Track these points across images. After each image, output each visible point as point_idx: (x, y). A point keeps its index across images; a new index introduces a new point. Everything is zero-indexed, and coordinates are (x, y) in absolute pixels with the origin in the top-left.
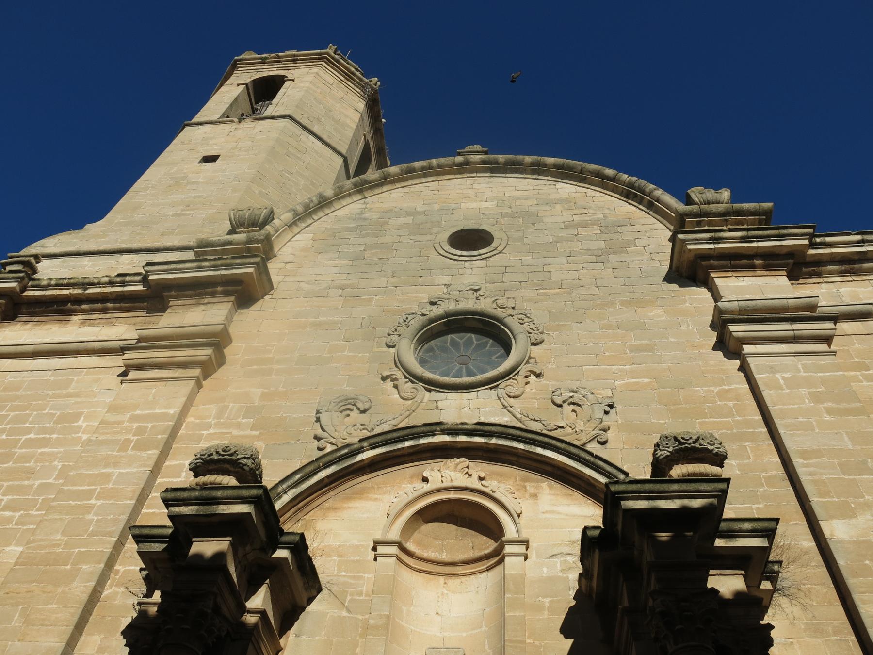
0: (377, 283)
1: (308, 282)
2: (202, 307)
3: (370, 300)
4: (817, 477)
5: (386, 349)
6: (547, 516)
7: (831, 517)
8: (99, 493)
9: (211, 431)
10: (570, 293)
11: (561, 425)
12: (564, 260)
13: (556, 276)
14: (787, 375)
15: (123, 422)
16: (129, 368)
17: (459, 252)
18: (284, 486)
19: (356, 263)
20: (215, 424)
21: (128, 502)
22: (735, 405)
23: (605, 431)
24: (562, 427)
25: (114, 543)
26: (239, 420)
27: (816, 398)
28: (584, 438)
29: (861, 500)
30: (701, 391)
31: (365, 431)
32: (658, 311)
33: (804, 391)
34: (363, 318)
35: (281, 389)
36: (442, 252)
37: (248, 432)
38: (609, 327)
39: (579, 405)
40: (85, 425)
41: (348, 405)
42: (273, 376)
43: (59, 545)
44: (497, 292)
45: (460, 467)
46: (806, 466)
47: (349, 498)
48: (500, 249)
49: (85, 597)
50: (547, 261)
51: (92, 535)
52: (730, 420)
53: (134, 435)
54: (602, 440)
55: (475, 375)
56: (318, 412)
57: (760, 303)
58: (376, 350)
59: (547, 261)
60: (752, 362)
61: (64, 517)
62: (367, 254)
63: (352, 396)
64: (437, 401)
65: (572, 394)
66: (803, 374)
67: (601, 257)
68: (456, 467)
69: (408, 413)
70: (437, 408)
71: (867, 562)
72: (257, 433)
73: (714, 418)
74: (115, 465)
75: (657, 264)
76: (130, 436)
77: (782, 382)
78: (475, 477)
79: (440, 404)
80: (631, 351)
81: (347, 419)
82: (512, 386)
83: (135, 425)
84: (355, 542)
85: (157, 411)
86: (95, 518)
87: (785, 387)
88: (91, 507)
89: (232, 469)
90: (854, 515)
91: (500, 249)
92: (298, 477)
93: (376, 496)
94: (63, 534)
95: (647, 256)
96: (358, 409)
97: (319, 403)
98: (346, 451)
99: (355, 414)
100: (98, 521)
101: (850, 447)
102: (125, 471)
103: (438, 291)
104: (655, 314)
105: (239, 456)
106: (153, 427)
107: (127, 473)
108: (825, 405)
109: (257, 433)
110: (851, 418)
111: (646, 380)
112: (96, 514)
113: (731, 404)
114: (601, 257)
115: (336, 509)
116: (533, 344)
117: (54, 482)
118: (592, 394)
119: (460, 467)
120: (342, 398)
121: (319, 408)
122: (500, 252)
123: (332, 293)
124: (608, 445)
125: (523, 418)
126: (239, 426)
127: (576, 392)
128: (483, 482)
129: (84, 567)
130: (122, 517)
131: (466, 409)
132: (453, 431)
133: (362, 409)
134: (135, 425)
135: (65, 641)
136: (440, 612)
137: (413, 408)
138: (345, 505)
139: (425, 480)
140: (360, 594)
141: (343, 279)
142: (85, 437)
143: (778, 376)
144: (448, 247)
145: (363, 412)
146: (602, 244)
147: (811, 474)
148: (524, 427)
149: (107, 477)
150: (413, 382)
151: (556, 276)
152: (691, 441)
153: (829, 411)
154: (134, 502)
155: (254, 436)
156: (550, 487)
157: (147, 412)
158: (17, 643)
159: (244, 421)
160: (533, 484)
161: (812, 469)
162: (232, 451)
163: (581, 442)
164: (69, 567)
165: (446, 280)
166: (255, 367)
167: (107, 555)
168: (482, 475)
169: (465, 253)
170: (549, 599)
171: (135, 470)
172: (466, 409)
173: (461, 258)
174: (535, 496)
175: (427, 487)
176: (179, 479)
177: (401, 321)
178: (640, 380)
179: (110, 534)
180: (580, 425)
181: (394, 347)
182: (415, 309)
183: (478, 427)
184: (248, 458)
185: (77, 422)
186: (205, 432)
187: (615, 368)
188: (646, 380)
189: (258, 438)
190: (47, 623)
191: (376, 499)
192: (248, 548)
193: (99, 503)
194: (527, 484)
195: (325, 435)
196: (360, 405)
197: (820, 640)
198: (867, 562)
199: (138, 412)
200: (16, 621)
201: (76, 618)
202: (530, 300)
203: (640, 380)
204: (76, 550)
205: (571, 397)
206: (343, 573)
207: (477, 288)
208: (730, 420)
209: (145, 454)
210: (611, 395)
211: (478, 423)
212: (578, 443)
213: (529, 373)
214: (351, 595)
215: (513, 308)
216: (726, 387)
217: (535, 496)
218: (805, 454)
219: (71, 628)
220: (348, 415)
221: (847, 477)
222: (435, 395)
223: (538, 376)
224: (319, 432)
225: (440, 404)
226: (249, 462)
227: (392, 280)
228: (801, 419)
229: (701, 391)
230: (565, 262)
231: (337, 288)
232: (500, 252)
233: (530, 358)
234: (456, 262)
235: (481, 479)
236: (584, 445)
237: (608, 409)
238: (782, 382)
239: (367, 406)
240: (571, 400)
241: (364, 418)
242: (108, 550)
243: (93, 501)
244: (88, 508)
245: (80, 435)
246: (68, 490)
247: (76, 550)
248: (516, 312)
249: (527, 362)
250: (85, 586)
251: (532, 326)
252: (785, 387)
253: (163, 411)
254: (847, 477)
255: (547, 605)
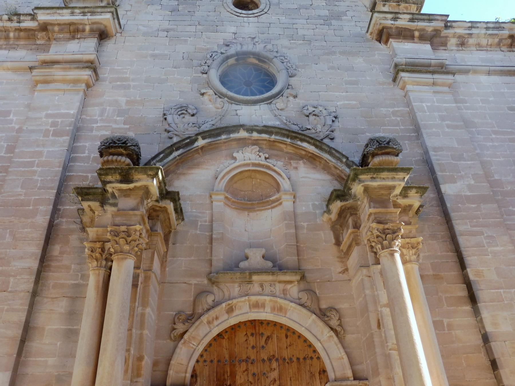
0: (189, 28)
1: (144, 26)
2: (77, 41)
3: (186, 41)
4: (440, 162)
5: (201, 75)
6: (303, 179)
7: (446, 183)
8: (38, 163)
9: (99, 125)
10: (310, 44)
11: (309, 128)
12: (304, 21)
13: (301, 32)
14: (429, 104)
15: (41, 118)
16: (37, 83)
17: (240, 11)
18: (154, 161)
19: (173, 13)
20: (100, 120)
21: (57, 169)
22: (401, 119)
23: (333, 132)
24: (309, 129)
25: (55, 194)
26: (115, 118)
27: (442, 118)
28: (322, 136)
29: (460, 174)
30: (384, 110)
31: (196, 128)
32: (360, 60)
33: (436, 114)
34: (184, 53)
35: (138, 98)
36: (229, 10)
37: (122, 126)
38: (332, 68)
39: (318, 116)
40: (15, 119)
41: (182, 110)
42: (131, 90)
43: (21, 195)
44: (266, 40)
45: (254, 151)
46: (436, 155)
47: (191, 168)
48: (266, 10)
49: (46, 224)
50: (295, 21)
51: (40, 188)
52: (398, 128)
53: (51, 127)
54: (332, 137)
55: (256, 95)
56: (164, 115)
57: (417, 61)
58: (194, 75)
59: (295, 21)
60: (412, 95)
61: (19, 178)
62: (181, 8)
63: (185, 105)
64: (236, 110)
65: (314, 109)
66: (436, 104)
67: (327, 21)
68: (252, 151)
69: (220, 117)
70: (237, 115)
71: (460, 205)
72: (128, 126)
73: (390, 126)
74: (44, 146)
75: (359, 29)
76: (48, 127)
77: (426, 108)
78: (263, 157)
79: (238, 112)
80: (346, 84)
81: (183, 120)
82: (279, 103)
83: (50, 120)
84: (199, 193)
85: (63, 111)
86: (40, 179)
87: (427, 111)
88: (35, 172)
89: (124, 152)
90: (455, 182)
91: (266, 10)
92: (162, 156)
93: (207, 167)
94: (22, 187)
95: (353, 24)
96: (189, 114)
97: (164, 108)
98: (188, 140)
99: (187, 117)
100: (41, 180)
101: (457, 146)
102: (50, 150)
103: (229, 37)
104: (359, 62)
105: (128, 145)
106: (62, 122)
107: (53, 151)
108: (446, 122)
109: (128, 126)
110: (458, 130)
111: (354, 102)
112: (39, 176)
113: (399, 119)
114: (327, 21)
115: (184, 174)
116: (290, 77)
117: (5, 155)
118: (326, 109)
119: (254, 151)
120: (179, 106)
121: (165, 112)
122: (266, 13)
123: (161, 34)
124: (334, 140)
125: (288, 123)
126: (116, 122)
127: (316, 108)
128: (268, 160)
129: (41, 207)
130: (56, 178)
131: (254, 116)
132: (250, 129)
133: (192, 114)
134: (50, 120)
135: (41, 249)
136: (247, 230)
137: (223, 114)
138: (189, 172)
139: (235, 159)
140: (206, 222)
141: (166, 25)
142: (17, 127)
143: (424, 104)
144: (232, 7)
145: (193, 115)
146: (327, 13)
147: (437, 160)
148: (289, 129)
149: (40, 153)
150: (220, 98)
151: (301, 32)
152: (385, 143)
153: (448, 126)
154: (61, 169)
155: (127, 129)
156: (304, 163)
157: (56, 112)
158: (12, 250)
159: (118, 118)
160: (294, 161)
161: (438, 157)
162: (124, 141)
163: (321, 138)
164: (31, 208)
165: (233, 29)
166: (118, 83)
167: (53, 201)
168: (267, 156)
169: (244, 12)
170: (307, 223)
171: (57, 149)
172: (254, 116)
173: (242, 15)
174: (296, 168)
175: (237, 164)
176: (85, 155)
177: (208, 56)
178: (351, 102)
179: (52, 188)
180: (319, 128)
181: (206, 73)
182: (216, 48)
183: (264, 128)
184: (134, 146)
185: (9, 116)
186: (95, 125)
187: (337, 94)
188: (354, 102)
189: (129, 129)
190: (27, 239)
191: (207, 169)
192: (149, 200)
193: (40, 169)
194: (292, 161)
195: (171, 129)
196: (190, 111)
197: (435, 242)
198: (460, 205)
199: (50, 112)
200: (8, 238)
201: (44, 237)
202: (286, 47)
203: (351, 102)
204: (33, 198)
205: (314, 111)
206: (195, 211)
207: (254, 36)
208: (398, 128)
209: (61, 139)
210: (335, 111)
211: (265, 126)
212: (319, 139)
213: (289, 95)
214: (200, 222)
215: (277, 52)
216: (396, 109)
217: (296, 168)
218: (436, 149)
219: (42, 242)
220: (184, 117)
221: (454, 162)
222: (234, 107)
223: (295, 97)
224: (167, 127)
225: (238, 112)
226: (136, 148)
227: (199, 27)
228: (434, 130)
229: (384, 110)
230: (306, 23)
231: (164, 31)
232: (266, 13)
233: (289, 85)
234: (238, 18)
235: (266, 158)
236: (322, 140)
237: (334, 119)
238: (426, 108)
239: (195, 111)
240: (314, 113)
241: (193, 119)
242: (53, 197)
243: (35, 168)
244: (34, 173)
245: (13, 125)
246: (17, 161)
247: (33, 198)
248: (279, 54)
249: (288, 88)
250: (44, 219)
251: (289, 65)
252: (427, 111)
253: (66, 111)
254: (454, 162)
255: (306, 226)
